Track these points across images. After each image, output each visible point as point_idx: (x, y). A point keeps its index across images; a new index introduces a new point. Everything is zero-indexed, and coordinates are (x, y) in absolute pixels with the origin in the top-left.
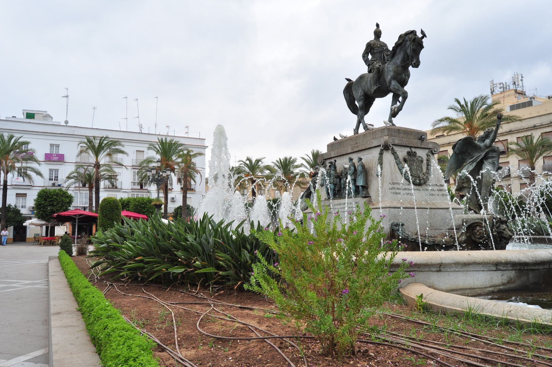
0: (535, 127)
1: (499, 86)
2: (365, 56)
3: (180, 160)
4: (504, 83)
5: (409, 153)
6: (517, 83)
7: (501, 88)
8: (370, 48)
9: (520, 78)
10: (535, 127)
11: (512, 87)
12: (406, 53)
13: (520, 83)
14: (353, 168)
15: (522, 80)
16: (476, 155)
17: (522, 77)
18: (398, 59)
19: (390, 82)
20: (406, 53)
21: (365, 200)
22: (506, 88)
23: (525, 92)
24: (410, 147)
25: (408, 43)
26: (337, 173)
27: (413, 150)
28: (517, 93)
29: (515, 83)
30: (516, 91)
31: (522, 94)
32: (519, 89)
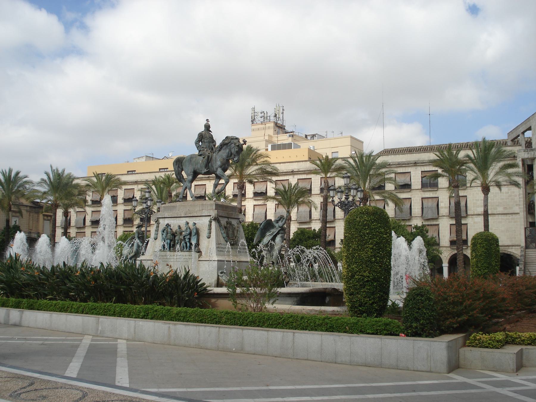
0: (293, 173)
1: (259, 114)
2: (197, 143)
3: (276, 269)
4: (265, 113)
5: (227, 223)
6: (277, 116)
7: (261, 117)
8: (201, 138)
9: (281, 111)
10: (293, 173)
11: (272, 118)
12: (230, 150)
13: (281, 117)
14: (189, 230)
15: (282, 113)
16: (272, 230)
17: (283, 110)
18: (224, 153)
19: (217, 169)
20: (230, 150)
21: (198, 254)
22: (267, 119)
23: (285, 126)
24: (228, 218)
25: (233, 145)
26: (49, 191)
27: (230, 220)
28: (277, 126)
29: (276, 116)
30: (276, 124)
31: (282, 128)
32: (279, 122)
